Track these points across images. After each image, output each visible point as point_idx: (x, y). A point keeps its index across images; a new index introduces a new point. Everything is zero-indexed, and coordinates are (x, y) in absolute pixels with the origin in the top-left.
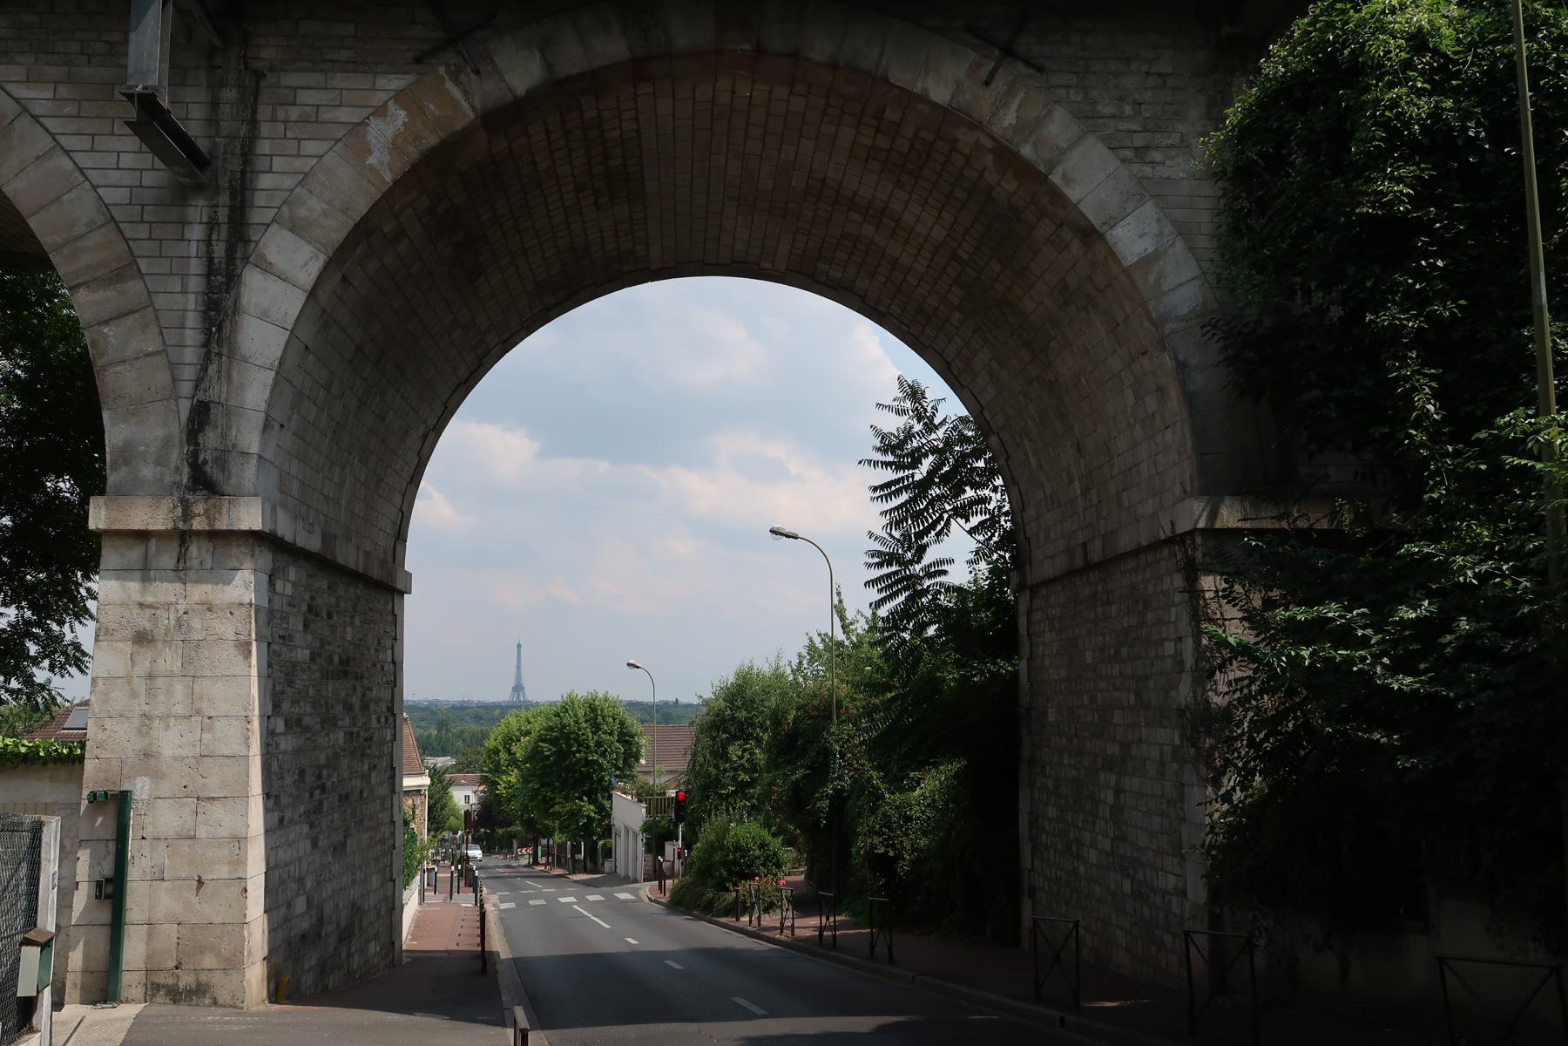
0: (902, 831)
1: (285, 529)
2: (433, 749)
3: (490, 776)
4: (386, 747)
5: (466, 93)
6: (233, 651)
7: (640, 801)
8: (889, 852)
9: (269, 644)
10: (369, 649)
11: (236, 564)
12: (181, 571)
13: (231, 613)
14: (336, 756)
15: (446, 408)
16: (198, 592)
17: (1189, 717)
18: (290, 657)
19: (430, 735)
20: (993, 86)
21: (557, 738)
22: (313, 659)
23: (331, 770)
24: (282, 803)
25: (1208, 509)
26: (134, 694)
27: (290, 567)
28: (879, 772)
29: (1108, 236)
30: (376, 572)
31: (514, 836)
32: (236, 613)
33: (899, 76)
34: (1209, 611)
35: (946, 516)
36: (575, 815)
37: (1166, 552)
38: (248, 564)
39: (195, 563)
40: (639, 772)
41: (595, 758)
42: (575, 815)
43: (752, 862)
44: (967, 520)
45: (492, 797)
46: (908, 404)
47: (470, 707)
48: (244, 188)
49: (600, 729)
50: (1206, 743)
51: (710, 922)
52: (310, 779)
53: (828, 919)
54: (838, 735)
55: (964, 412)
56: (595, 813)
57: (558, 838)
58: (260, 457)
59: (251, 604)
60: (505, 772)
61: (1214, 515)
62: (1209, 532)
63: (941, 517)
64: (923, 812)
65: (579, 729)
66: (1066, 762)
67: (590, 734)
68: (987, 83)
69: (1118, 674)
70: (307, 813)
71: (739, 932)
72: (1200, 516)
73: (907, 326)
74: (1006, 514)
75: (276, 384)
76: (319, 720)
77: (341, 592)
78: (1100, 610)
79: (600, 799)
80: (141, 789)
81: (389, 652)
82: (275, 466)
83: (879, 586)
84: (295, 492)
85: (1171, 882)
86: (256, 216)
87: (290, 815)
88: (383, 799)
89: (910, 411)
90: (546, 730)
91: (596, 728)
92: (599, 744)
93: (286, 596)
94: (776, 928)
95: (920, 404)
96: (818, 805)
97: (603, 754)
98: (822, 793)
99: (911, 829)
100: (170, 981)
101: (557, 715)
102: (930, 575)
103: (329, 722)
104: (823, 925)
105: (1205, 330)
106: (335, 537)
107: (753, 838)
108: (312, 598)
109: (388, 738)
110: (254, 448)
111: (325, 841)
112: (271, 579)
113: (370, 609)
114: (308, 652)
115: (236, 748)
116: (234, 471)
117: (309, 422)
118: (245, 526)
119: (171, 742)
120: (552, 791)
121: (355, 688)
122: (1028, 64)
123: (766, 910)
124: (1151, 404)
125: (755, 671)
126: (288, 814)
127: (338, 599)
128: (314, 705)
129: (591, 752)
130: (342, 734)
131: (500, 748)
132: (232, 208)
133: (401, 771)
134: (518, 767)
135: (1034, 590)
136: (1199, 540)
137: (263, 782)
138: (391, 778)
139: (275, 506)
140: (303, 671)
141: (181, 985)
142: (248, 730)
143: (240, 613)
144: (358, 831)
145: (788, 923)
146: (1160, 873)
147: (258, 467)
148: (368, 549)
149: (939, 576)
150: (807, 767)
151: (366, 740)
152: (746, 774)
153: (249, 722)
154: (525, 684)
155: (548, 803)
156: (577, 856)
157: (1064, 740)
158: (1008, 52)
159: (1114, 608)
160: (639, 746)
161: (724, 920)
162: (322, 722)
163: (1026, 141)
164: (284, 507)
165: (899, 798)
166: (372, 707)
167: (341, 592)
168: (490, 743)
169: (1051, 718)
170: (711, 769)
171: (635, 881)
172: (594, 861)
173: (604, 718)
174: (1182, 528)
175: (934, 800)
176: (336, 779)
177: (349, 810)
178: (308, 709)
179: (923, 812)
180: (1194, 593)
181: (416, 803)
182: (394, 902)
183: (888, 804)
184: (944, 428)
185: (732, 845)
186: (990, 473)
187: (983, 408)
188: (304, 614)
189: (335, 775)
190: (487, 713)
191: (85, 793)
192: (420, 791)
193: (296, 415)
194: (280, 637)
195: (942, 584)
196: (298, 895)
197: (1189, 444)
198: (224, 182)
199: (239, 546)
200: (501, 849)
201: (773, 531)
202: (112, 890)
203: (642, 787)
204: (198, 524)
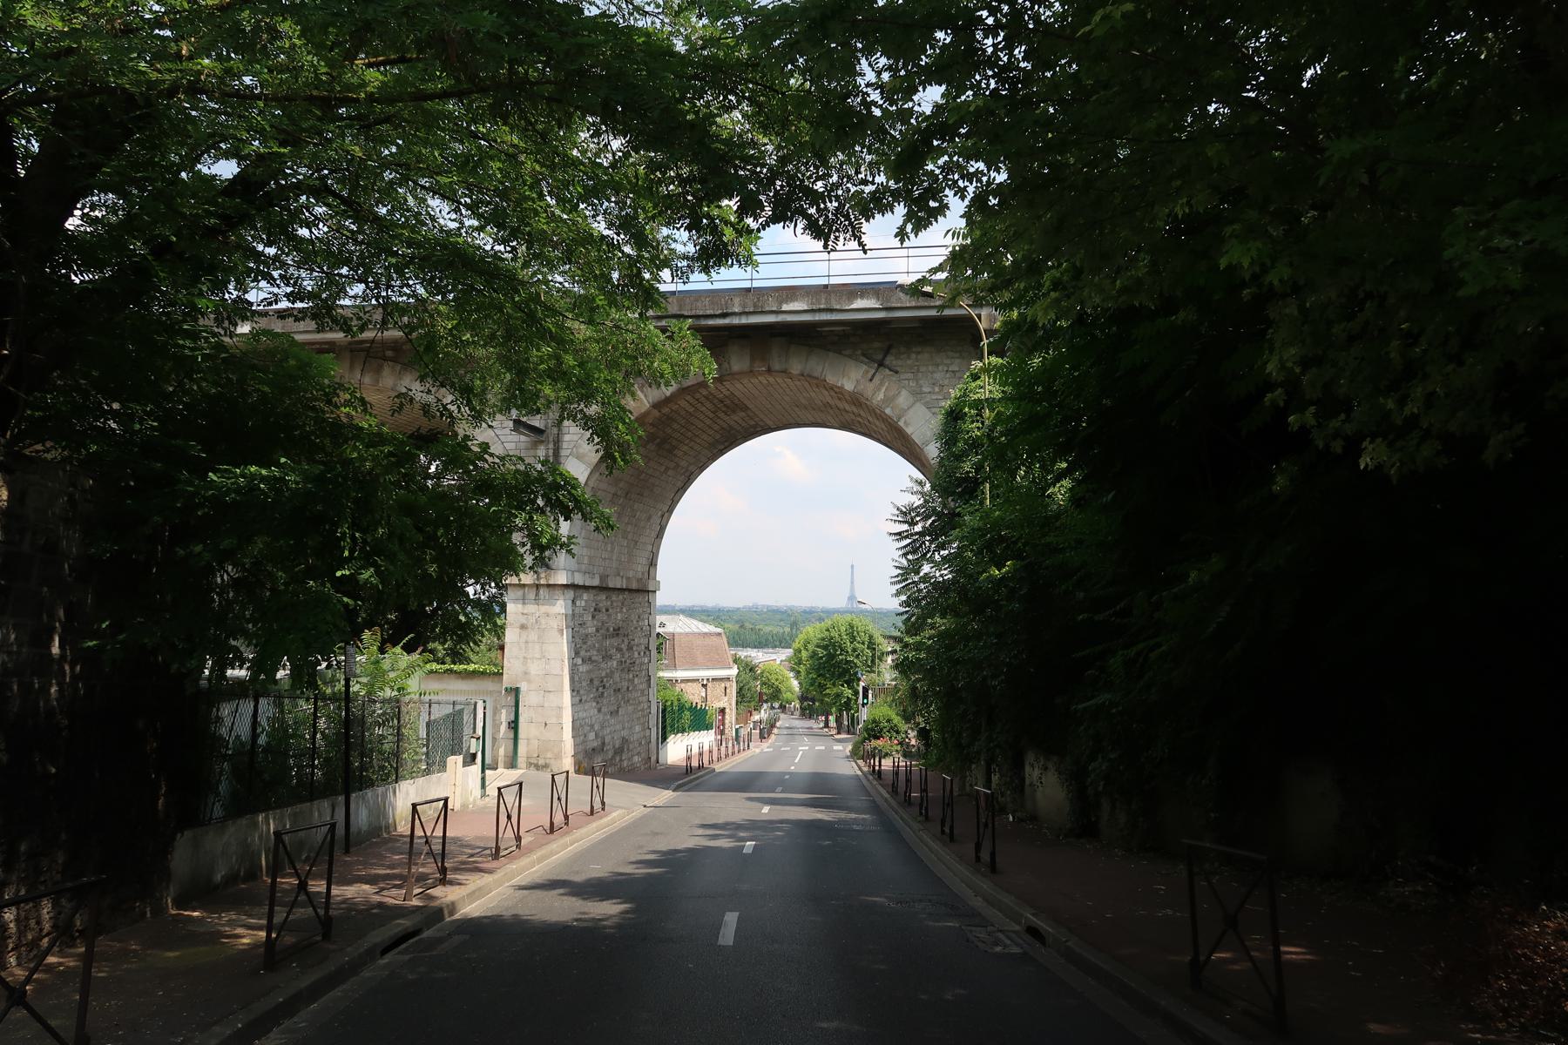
1: (579, 580)
5: (645, 396)
6: (557, 633)
10: (632, 621)
12: (537, 599)
14: (612, 672)
16: (544, 609)
20: (874, 381)
22: (597, 631)
26: (520, 649)
29: (925, 450)
33: (831, 379)
36: (838, 696)
38: (562, 597)
39: (542, 597)
43: (882, 730)
48: (558, 441)
52: (596, 683)
65: (841, 640)
67: (849, 644)
68: (871, 380)
70: (595, 698)
77: (614, 598)
80: (524, 687)
86: (563, 453)
88: (643, 691)
91: (853, 639)
92: (854, 650)
97: (857, 656)
100: (536, 762)
101: (828, 630)
103: (607, 657)
109: (646, 661)
112: (573, 602)
119: (535, 668)
121: (623, 641)
122: (891, 370)
126: (584, 698)
127: (612, 602)
128: (598, 651)
130: (615, 663)
132: (554, 450)
140: (592, 637)
141: (540, 763)
155: (822, 687)
158: (881, 364)
163: (888, 407)
178: (595, 653)
191: (504, 687)
193: (584, 531)
196: (590, 732)
198: (551, 439)
202: (514, 725)
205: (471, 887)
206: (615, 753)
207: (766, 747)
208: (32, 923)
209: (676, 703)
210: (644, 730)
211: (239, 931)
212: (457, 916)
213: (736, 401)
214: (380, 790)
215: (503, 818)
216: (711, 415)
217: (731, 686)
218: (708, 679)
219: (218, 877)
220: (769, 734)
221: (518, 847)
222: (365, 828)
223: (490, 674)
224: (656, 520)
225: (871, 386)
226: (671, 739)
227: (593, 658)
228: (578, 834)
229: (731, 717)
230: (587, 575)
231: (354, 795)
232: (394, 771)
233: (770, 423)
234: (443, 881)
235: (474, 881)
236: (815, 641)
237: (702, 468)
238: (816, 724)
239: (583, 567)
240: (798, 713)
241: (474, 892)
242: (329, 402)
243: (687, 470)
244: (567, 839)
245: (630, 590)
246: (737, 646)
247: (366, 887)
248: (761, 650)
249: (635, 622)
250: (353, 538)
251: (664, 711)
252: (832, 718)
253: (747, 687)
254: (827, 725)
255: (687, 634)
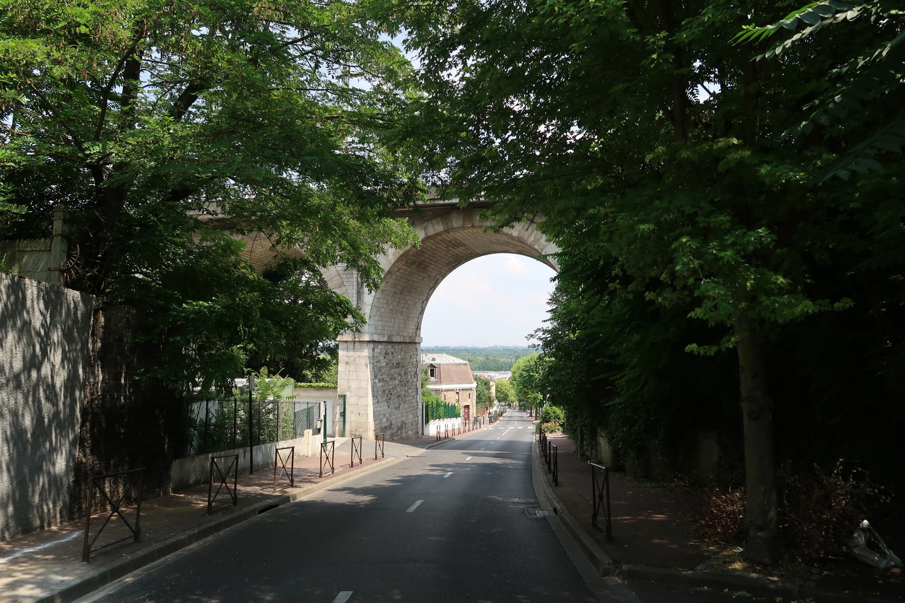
1: (376, 338)
12: (354, 349)
14: (395, 386)
16: (358, 354)
22: (387, 365)
26: (346, 374)
36: (535, 398)
43: (550, 418)
52: (387, 392)
68: (527, 230)
70: (386, 400)
80: (348, 394)
101: (529, 361)
103: (393, 378)
109: (415, 380)
115: (366, 387)
119: (353, 385)
126: (380, 400)
128: (388, 375)
130: (397, 382)
143: (366, 358)
202: (343, 414)
204: (357, 339)
205: (305, 489)
206: (398, 429)
207: (491, 427)
208: (116, 493)
209: (435, 402)
210: (414, 417)
211: (199, 502)
212: (296, 501)
213: (458, 242)
214: (269, 445)
215: (324, 459)
216: (446, 249)
219: (191, 481)
220: (496, 420)
221: (333, 472)
222: (261, 463)
223: (331, 388)
224: (419, 305)
225: (527, 233)
226: (432, 422)
227: (385, 379)
228: (365, 468)
229: (473, 411)
230: (381, 336)
231: (255, 447)
232: (273, 438)
233: (479, 252)
234: (292, 486)
235: (307, 486)
236: (521, 369)
237: (444, 276)
238: (525, 415)
239: (379, 331)
240: (517, 408)
241: (306, 491)
242: (235, 267)
243: (435, 278)
244: (359, 470)
245: (405, 343)
246: (484, 370)
247: (258, 488)
248: (498, 372)
250: (245, 331)
251: (427, 407)
252: (534, 411)
253: (482, 394)
254: (531, 416)
255: (447, 364)
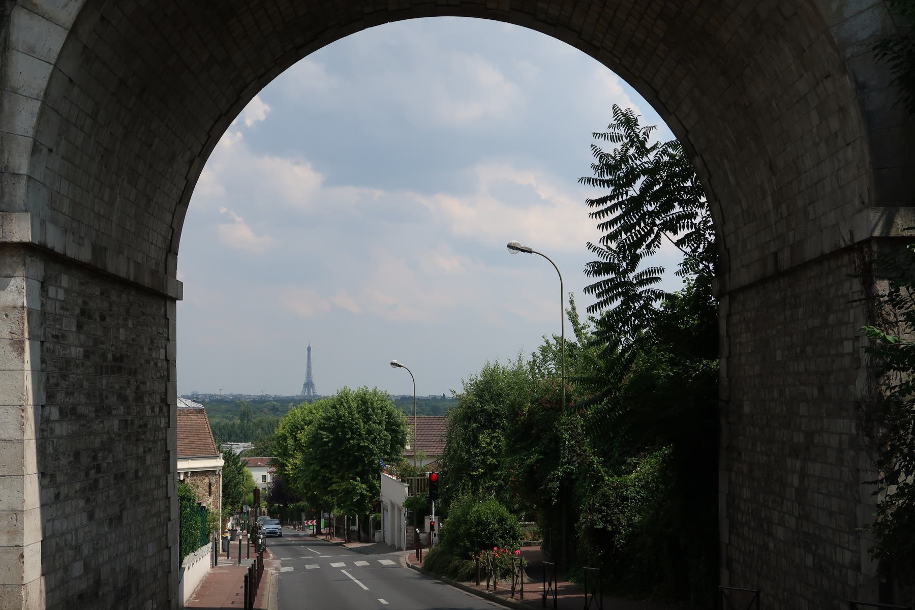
0: (618, 509)
1: (55, 240)
2: (237, 436)
3: (280, 459)
4: (160, 433)
6: (8, 349)
7: (403, 481)
8: (607, 527)
9: (42, 343)
10: (142, 348)
11: (9, 272)
13: (7, 316)
15: (210, 136)
17: (864, 409)
18: (65, 354)
19: (234, 424)
21: (334, 427)
22: (87, 355)
23: (106, 453)
24: (58, 482)
25: (883, 219)
27: (62, 274)
28: (599, 458)
30: (147, 281)
31: (303, 510)
32: (11, 315)
34: (884, 312)
35: (656, 229)
37: (846, 259)
38: (21, 272)
40: (404, 457)
41: (366, 444)
42: (349, 492)
43: (492, 534)
44: (675, 233)
45: (281, 477)
46: (622, 131)
47: (268, 401)
49: (370, 419)
50: (879, 433)
51: (455, 586)
52: (85, 460)
53: (550, 585)
54: (568, 425)
55: (672, 137)
56: (367, 491)
57: (336, 512)
58: (29, 178)
59: (23, 307)
60: (292, 456)
61: (889, 224)
62: (885, 240)
63: (652, 231)
64: (638, 493)
65: (353, 419)
66: (759, 449)
69: (803, 370)
71: (478, 595)
72: (876, 225)
73: (619, 58)
74: (711, 228)
75: (42, 114)
76: (94, 409)
77: (114, 298)
78: (788, 313)
79: (371, 479)
81: (163, 351)
82: (46, 186)
83: (597, 291)
84: (65, 209)
85: (847, 557)
87: (66, 492)
89: (624, 138)
90: (324, 419)
91: (367, 418)
92: (369, 432)
93: (58, 300)
94: (507, 592)
95: (633, 130)
96: (550, 485)
97: (373, 441)
98: (553, 475)
99: (627, 507)
101: (334, 407)
102: (642, 283)
103: (103, 411)
104: (546, 590)
105: (876, 51)
106: (105, 249)
107: (493, 514)
108: (85, 303)
109: (163, 425)
110: (24, 170)
111: (101, 515)
113: (143, 313)
114: (82, 350)
115: (17, 435)
116: (6, 190)
117: (77, 148)
118: (16, 239)
120: (330, 472)
121: (129, 382)
123: (503, 576)
124: (834, 124)
125: (501, 369)
126: (64, 491)
129: (363, 439)
130: (116, 422)
131: (288, 435)
133: (175, 455)
134: (303, 451)
135: (732, 295)
136: (875, 248)
137: (39, 463)
138: (165, 460)
139: (44, 221)
140: (77, 366)
142: (22, 417)
144: (134, 505)
145: (518, 588)
146: (838, 549)
147: (28, 187)
148: (140, 261)
149: (651, 282)
150: (541, 453)
151: (140, 426)
152: (494, 458)
153: (23, 411)
154: (315, 380)
155: (327, 482)
156: (352, 528)
157: (757, 430)
159: (801, 311)
160: (404, 435)
161: (466, 584)
162: (97, 411)
164: (54, 222)
165: (617, 480)
166: (146, 399)
167: (114, 298)
168: (279, 431)
169: (747, 410)
170: (464, 454)
171: (400, 549)
172: (366, 531)
173: (373, 410)
174: (860, 236)
175: (647, 483)
176: (111, 461)
177: (125, 488)
178: (83, 399)
179: (638, 493)
180: (870, 297)
181: (212, 481)
182: (170, 566)
183: (607, 485)
184: (655, 152)
185: (475, 520)
186: (696, 191)
187: (688, 132)
188: (78, 316)
189: (111, 456)
190: (280, 405)
192: (214, 471)
193: (63, 141)
194: (53, 336)
195: (653, 292)
197: (868, 159)
199: (12, 256)
200: (292, 521)
201: (510, 246)
203: (405, 469)
217: (217, 482)
218: (186, 474)
249: (146, 350)
